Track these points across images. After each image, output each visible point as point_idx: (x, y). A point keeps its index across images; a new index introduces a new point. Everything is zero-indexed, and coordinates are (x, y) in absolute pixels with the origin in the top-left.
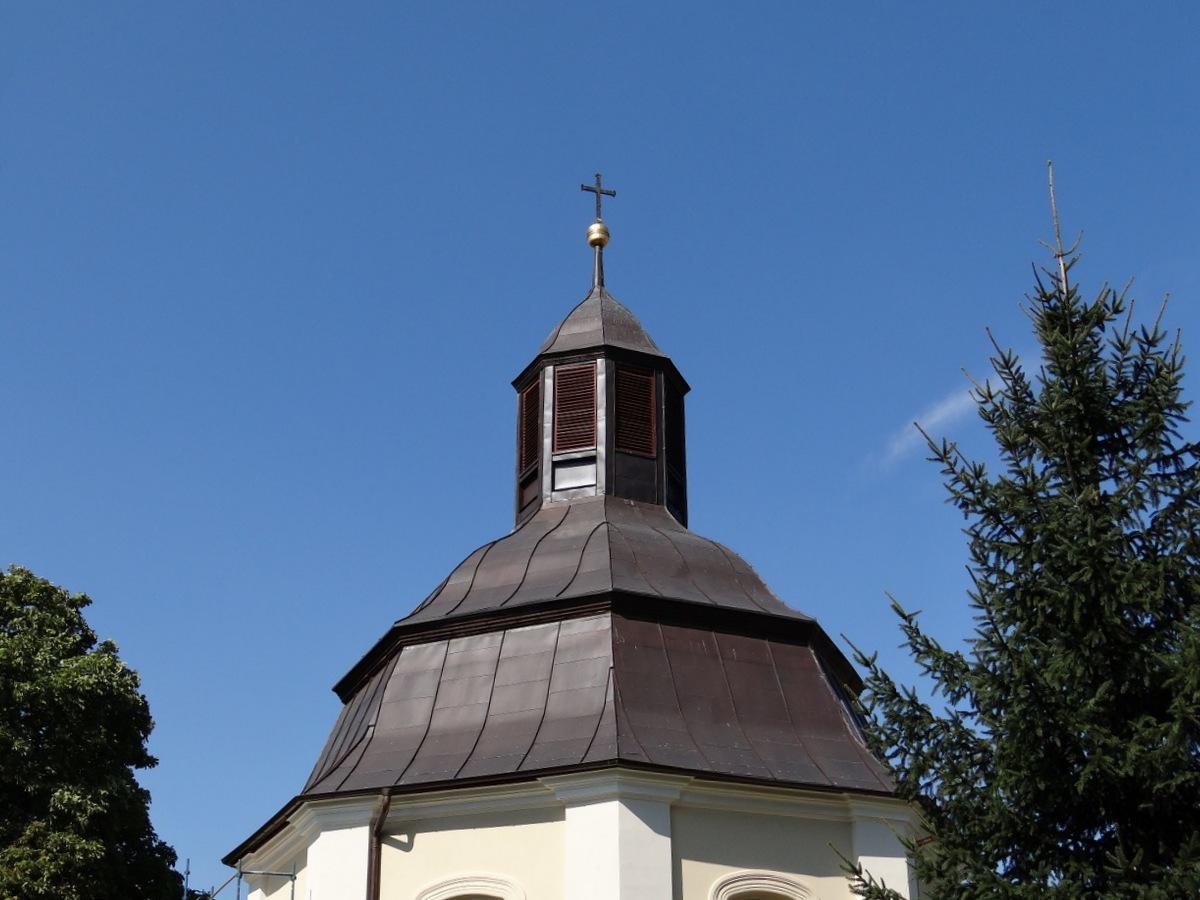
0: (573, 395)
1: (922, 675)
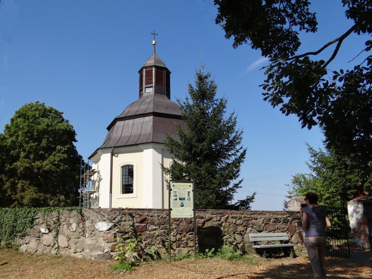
0: (149, 74)
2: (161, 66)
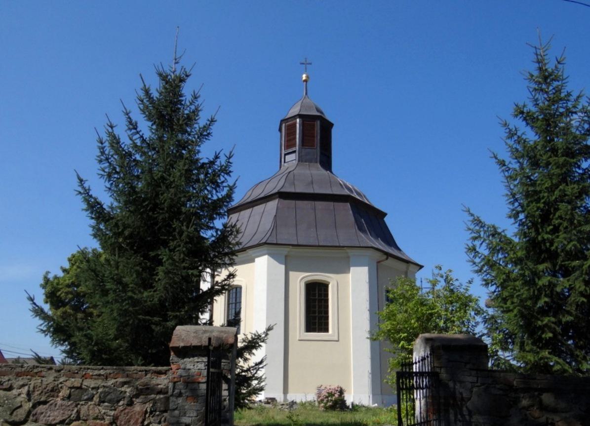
1: (83, 210)
2: (307, 114)
